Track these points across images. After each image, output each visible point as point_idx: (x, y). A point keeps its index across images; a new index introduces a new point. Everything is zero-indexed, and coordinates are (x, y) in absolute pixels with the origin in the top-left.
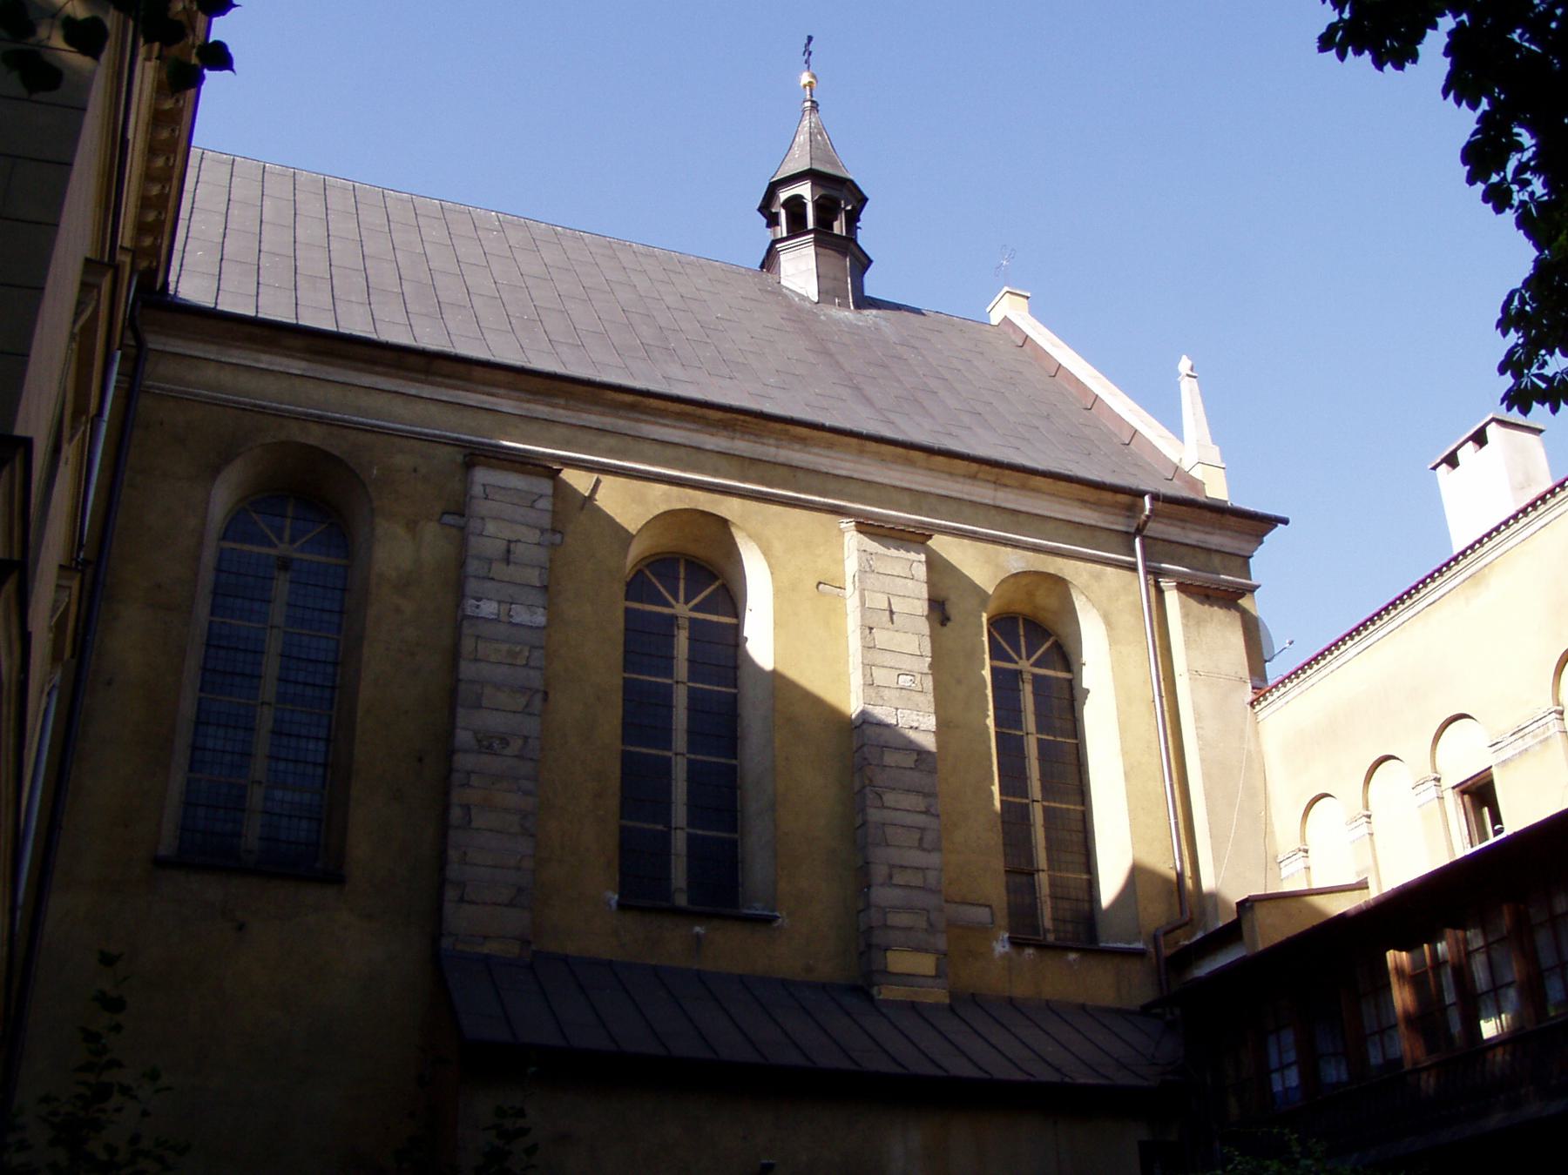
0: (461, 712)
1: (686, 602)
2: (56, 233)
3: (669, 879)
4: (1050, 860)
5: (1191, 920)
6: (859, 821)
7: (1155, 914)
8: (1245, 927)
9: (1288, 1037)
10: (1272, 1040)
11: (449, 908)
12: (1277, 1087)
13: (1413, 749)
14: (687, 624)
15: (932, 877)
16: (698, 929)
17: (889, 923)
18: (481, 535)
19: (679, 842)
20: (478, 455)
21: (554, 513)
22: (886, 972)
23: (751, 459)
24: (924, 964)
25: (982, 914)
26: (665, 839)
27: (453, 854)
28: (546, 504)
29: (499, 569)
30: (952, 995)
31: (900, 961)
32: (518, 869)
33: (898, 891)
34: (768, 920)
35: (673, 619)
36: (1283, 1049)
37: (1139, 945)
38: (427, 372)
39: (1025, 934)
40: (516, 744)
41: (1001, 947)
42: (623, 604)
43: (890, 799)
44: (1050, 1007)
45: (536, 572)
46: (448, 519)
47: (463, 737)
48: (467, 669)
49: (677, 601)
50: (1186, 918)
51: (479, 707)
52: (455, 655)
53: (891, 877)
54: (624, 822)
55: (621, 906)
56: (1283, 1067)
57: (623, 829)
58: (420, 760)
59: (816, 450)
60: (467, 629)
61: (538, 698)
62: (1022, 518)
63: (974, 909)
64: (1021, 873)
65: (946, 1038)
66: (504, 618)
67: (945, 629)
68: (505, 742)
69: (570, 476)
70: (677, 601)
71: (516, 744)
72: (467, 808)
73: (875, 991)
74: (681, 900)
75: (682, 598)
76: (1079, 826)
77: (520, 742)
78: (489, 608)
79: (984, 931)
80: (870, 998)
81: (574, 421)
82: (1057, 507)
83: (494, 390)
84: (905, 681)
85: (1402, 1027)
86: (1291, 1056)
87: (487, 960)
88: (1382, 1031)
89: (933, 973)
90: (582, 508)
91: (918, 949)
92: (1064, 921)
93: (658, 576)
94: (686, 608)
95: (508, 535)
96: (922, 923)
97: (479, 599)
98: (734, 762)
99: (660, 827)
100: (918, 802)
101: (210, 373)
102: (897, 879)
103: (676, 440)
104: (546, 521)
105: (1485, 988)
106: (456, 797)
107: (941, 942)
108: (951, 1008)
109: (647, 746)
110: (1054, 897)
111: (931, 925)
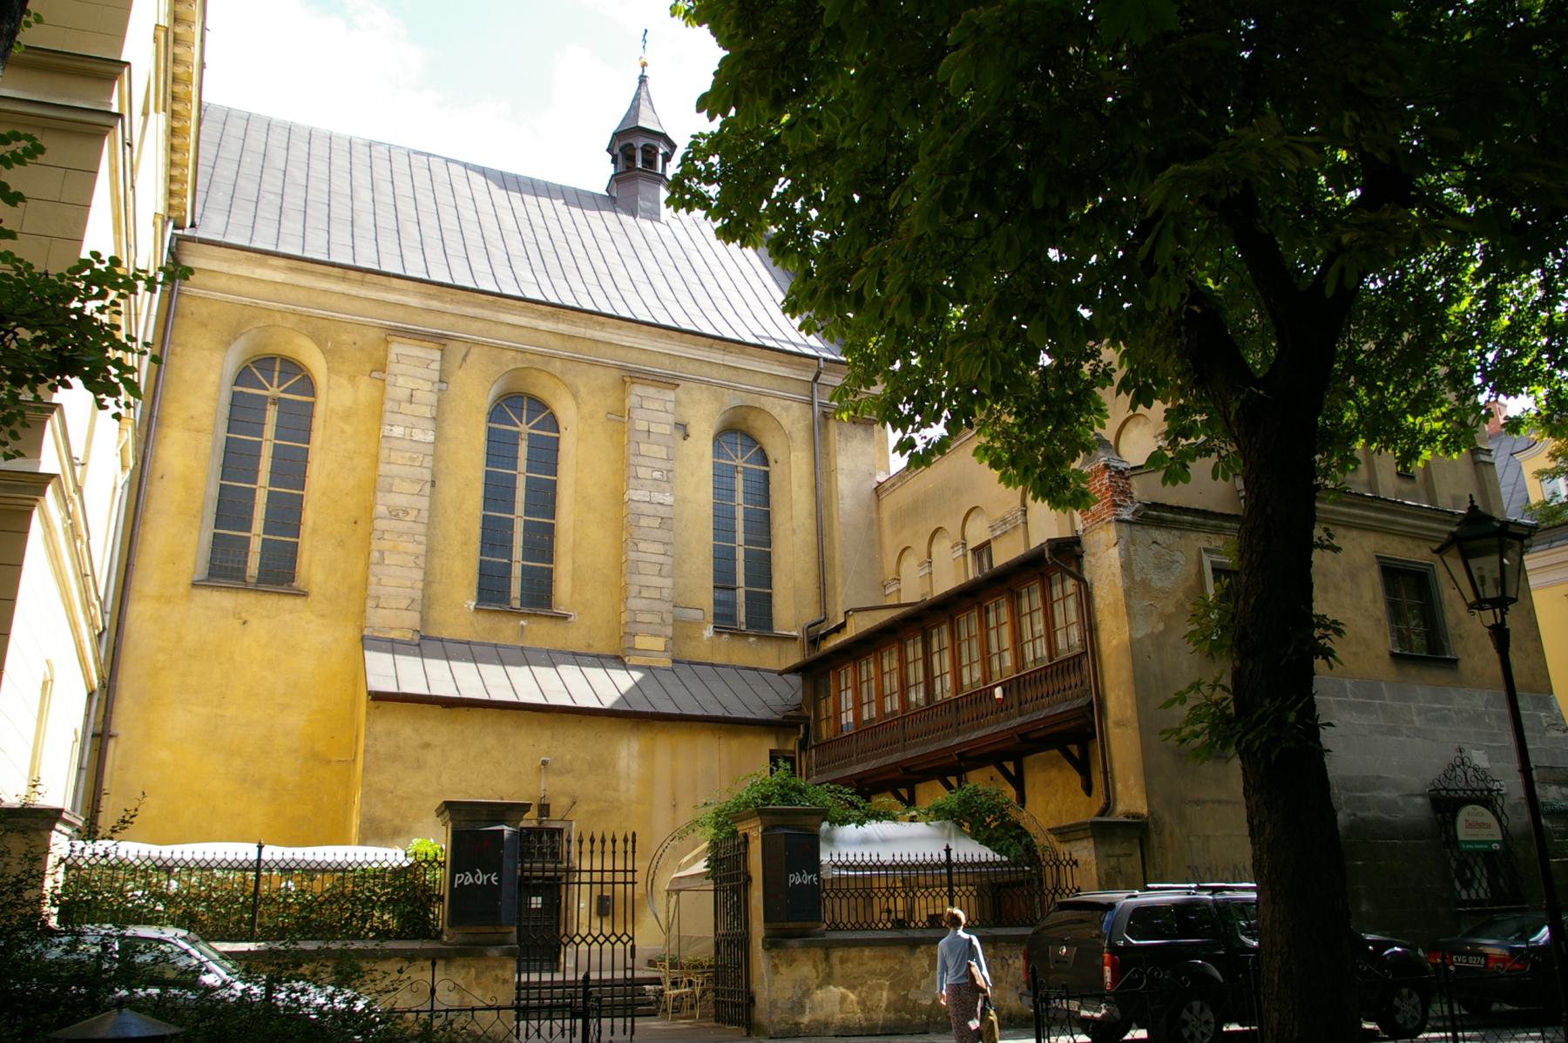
0: (379, 494)
1: (527, 424)
2: (81, 244)
3: (509, 592)
6: (624, 559)
11: (370, 611)
12: (844, 722)
13: (952, 526)
14: (527, 437)
16: (522, 622)
19: (517, 571)
21: (441, 371)
22: (633, 648)
23: (569, 336)
25: (698, 614)
26: (508, 567)
27: (373, 579)
28: (436, 366)
29: (405, 407)
31: (642, 642)
32: (412, 588)
33: (644, 601)
34: (565, 617)
35: (517, 435)
40: (413, 514)
41: (708, 632)
42: (299, 540)
43: (642, 546)
46: (375, 374)
47: (381, 510)
48: (384, 469)
49: (521, 422)
51: (391, 491)
52: (376, 459)
53: (640, 592)
54: (483, 558)
58: (355, 523)
59: (609, 330)
60: (384, 444)
61: (428, 487)
62: (740, 371)
66: (408, 437)
67: (686, 442)
68: (406, 513)
70: (521, 422)
71: (413, 514)
72: (382, 553)
73: (626, 659)
74: (516, 604)
75: (524, 421)
77: (416, 512)
78: (398, 431)
79: (699, 624)
81: (456, 312)
82: (764, 365)
84: (657, 475)
93: (511, 407)
94: (527, 427)
97: (392, 426)
98: (553, 521)
99: (506, 561)
101: (222, 282)
103: (522, 324)
104: (436, 377)
105: (975, 665)
106: (375, 545)
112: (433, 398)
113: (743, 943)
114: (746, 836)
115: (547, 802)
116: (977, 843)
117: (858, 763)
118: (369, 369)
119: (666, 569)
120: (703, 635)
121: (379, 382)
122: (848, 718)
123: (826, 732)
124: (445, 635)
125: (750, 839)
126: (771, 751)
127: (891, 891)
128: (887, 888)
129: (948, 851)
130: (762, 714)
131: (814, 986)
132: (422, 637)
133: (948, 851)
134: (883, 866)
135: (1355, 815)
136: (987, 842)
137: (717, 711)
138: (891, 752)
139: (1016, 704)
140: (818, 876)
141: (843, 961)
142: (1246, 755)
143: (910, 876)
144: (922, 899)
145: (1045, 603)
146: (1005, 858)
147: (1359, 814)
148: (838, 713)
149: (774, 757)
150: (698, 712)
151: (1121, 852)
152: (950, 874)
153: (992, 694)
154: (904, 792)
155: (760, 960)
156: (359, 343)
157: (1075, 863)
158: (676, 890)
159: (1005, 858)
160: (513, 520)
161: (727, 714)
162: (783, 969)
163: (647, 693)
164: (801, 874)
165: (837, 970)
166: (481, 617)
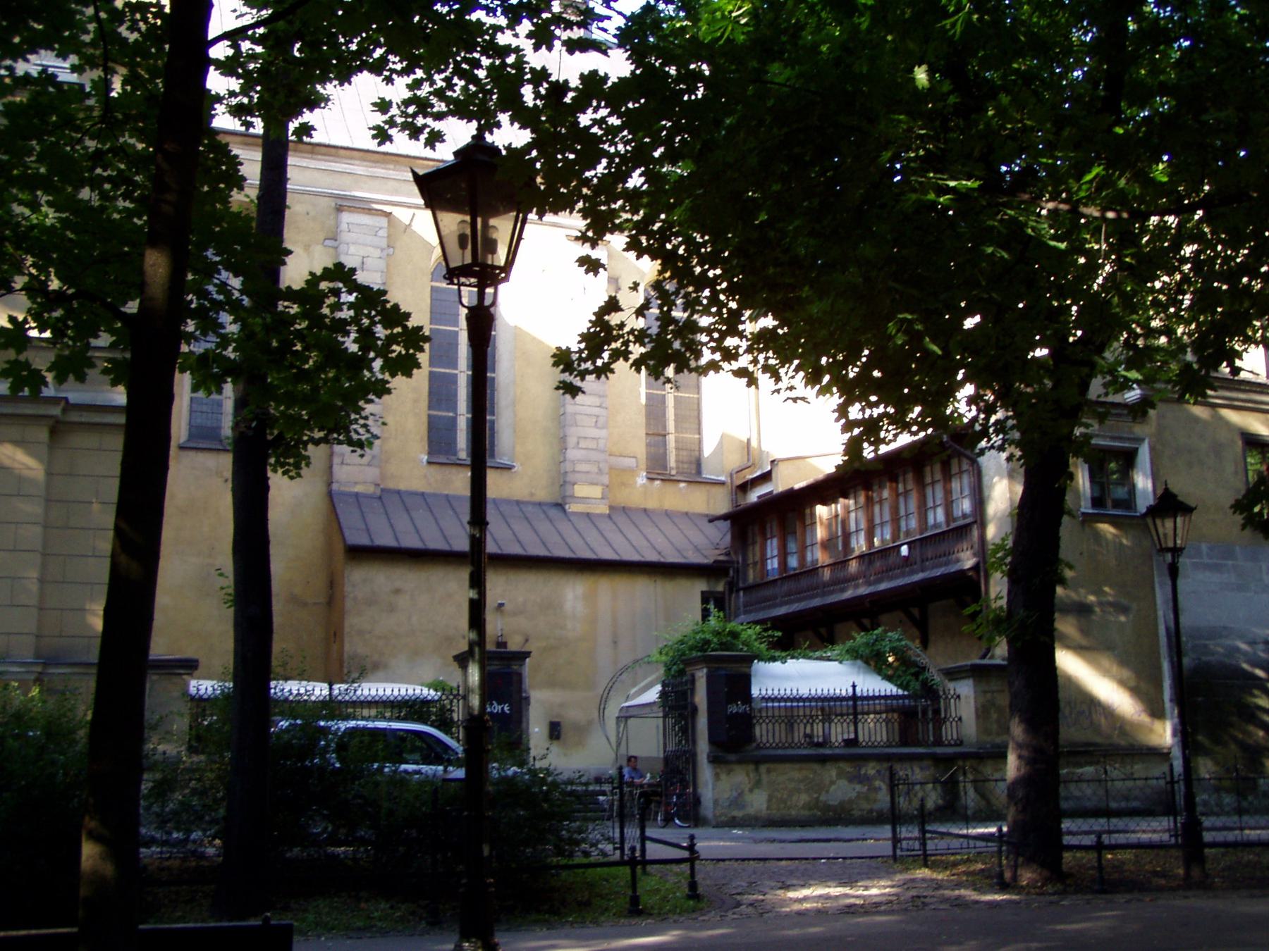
4: (676, 427)
5: (753, 464)
7: (733, 460)
8: (774, 475)
9: (775, 541)
10: (769, 542)
11: (336, 468)
12: (769, 567)
15: (602, 443)
17: (577, 469)
18: (347, 254)
20: (343, 205)
21: (389, 236)
22: (573, 496)
24: (596, 492)
25: (631, 462)
28: (383, 233)
30: (611, 508)
33: (583, 452)
34: (509, 468)
36: (773, 547)
37: (723, 478)
38: (312, 152)
39: (657, 469)
41: (641, 480)
44: (668, 514)
45: (379, 274)
46: (327, 242)
50: (750, 464)
53: (578, 443)
55: (429, 463)
56: (773, 557)
57: (430, 416)
63: (626, 459)
64: (659, 435)
65: (602, 535)
69: (398, 212)
73: (567, 507)
76: (696, 407)
79: (632, 472)
80: (564, 511)
83: (352, 162)
85: (818, 546)
86: (775, 552)
87: (357, 495)
88: (812, 545)
89: (600, 496)
90: (405, 232)
91: (592, 484)
92: (682, 462)
95: (362, 253)
96: (595, 469)
99: (451, 414)
100: (597, 401)
102: (582, 445)
104: (384, 243)
107: (606, 480)
108: (609, 516)
109: (445, 325)
110: (677, 449)
111: (600, 470)
112: (382, 264)
113: (691, 757)
114: (693, 676)
115: (504, 640)
116: (880, 678)
117: (781, 605)
118: (322, 238)
119: (601, 420)
120: (636, 482)
121: (332, 250)
122: (773, 564)
123: (752, 576)
124: (402, 486)
125: (697, 677)
126: (703, 593)
127: (811, 719)
128: (805, 716)
129: (854, 686)
130: (694, 558)
131: (747, 789)
132: (383, 490)
133: (854, 686)
134: (801, 699)
135: (1199, 659)
136: (889, 678)
137: (652, 557)
138: (812, 597)
139: (918, 560)
140: (750, 706)
141: (769, 771)
142: (1007, 637)
143: (827, 707)
144: (839, 724)
145: (919, 508)
146: (906, 693)
147: (1204, 658)
148: (764, 560)
149: (705, 598)
150: (635, 557)
151: (995, 688)
152: (855, 706)
153: (899, 551)
154: (823, 631)
155: (706, 772)
156: (312, 213)
157: (959, 697)
158: (626, 716)
159: (906, 693)
160: (456, 375)
161: (662, 560)
162: (723, 777)
163: (588, 539)
164: (492, 704)
165: (765, 778)
166: (433, 470)
